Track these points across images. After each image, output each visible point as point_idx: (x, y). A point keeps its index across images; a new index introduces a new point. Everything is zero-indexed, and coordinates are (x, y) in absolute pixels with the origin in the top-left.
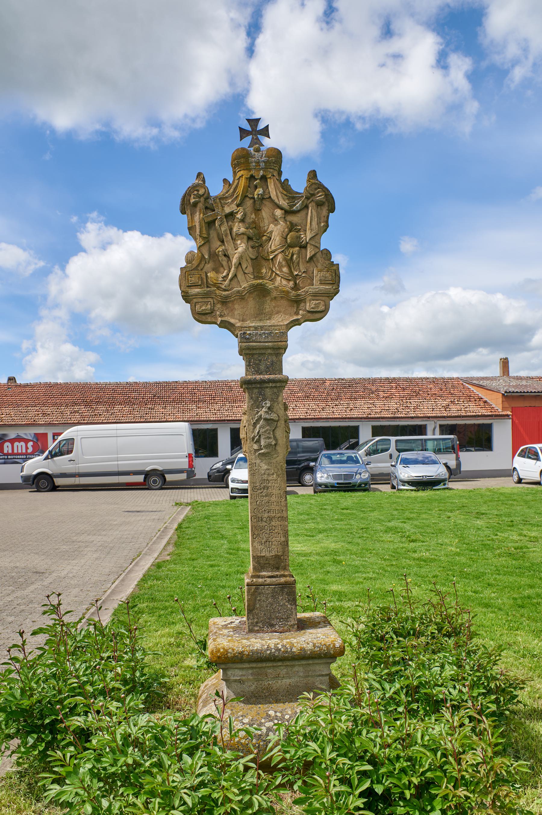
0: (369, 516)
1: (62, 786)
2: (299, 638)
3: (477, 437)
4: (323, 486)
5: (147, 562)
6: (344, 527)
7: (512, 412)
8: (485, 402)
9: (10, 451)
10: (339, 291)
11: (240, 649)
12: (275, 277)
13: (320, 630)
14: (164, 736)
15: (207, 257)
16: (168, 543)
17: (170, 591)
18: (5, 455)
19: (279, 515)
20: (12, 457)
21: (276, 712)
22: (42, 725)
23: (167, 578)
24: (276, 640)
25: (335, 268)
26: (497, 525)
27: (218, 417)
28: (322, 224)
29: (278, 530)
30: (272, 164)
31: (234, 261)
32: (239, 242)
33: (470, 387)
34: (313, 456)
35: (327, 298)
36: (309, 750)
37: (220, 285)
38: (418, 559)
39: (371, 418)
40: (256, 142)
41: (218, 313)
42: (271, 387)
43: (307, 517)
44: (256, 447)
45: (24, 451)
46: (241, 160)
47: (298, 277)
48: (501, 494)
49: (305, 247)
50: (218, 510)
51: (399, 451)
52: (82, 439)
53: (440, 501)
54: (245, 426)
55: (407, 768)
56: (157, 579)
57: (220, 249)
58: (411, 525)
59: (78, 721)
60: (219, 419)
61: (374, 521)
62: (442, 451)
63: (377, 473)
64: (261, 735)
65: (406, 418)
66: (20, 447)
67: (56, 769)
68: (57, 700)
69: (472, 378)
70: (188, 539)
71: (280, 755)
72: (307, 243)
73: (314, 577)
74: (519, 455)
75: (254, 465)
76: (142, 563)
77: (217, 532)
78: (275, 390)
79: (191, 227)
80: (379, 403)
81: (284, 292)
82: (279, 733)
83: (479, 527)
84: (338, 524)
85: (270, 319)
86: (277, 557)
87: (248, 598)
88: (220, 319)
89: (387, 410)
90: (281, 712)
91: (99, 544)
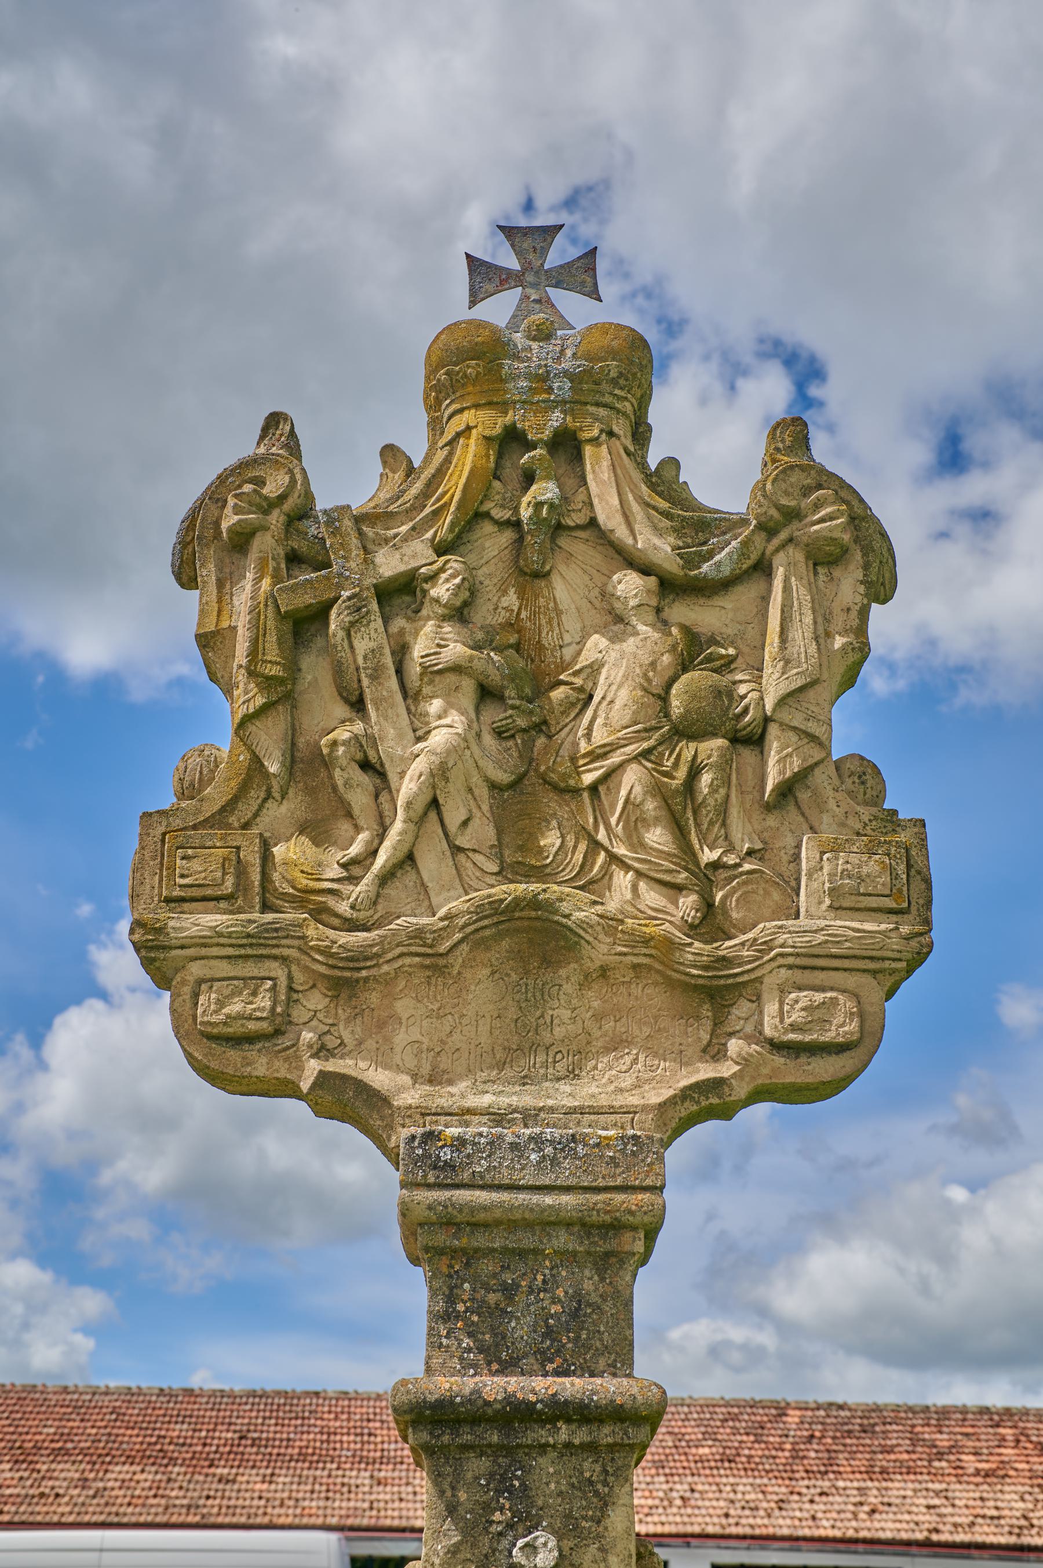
42: (568, 1445)
78: (590, 1468)
80: (964, 1494)
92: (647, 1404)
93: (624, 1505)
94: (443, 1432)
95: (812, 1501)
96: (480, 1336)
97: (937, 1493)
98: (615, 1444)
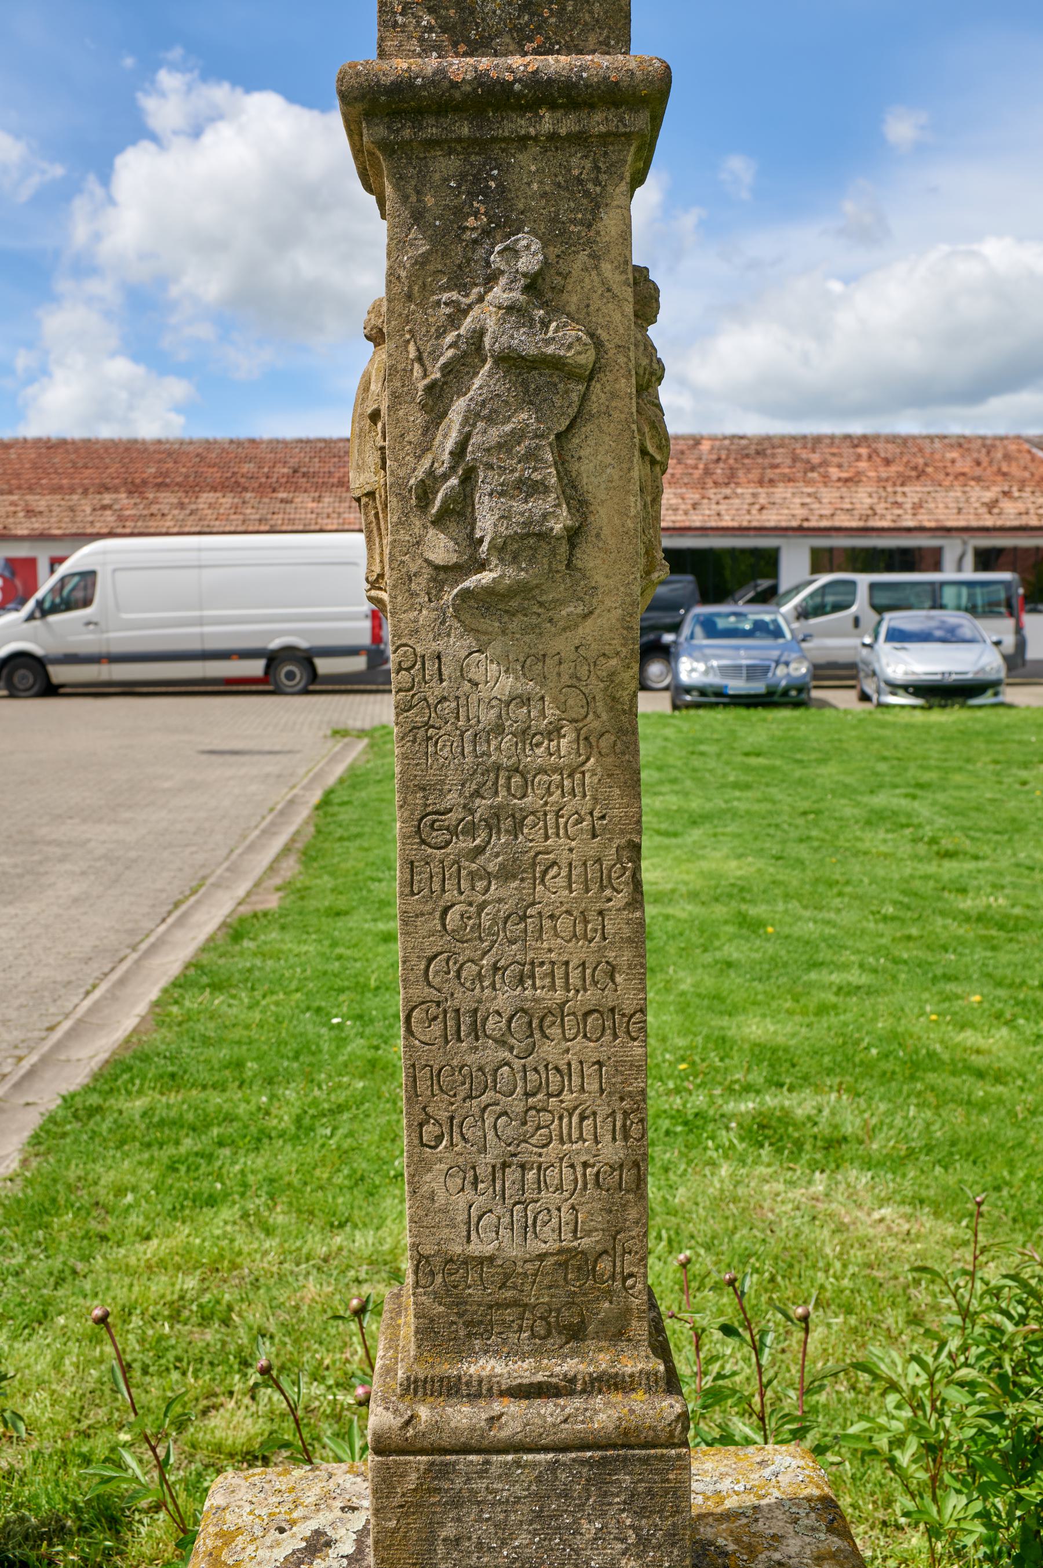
0: (818, 775)
6: (756, 807)
16: (286, 850)
19: (590, 997)
34: (668, 619)
42: (553, 137)
44: (441, 548)
51: (880, 609)
52: (118, 574)
53: (990, 735)
62: (980, 609)
70: (341, 839)
75: (431, 668)
76: (198, 917)
78: (579, 164)
80: (828, 495)
84: (739, 799)
86: (572, 1262)
92: (648, 81)
93: (619, 207)
94: (403, 126)
95: (718, 503)
96: (443, 12)
97: (809, 495)
98: (608, 134)
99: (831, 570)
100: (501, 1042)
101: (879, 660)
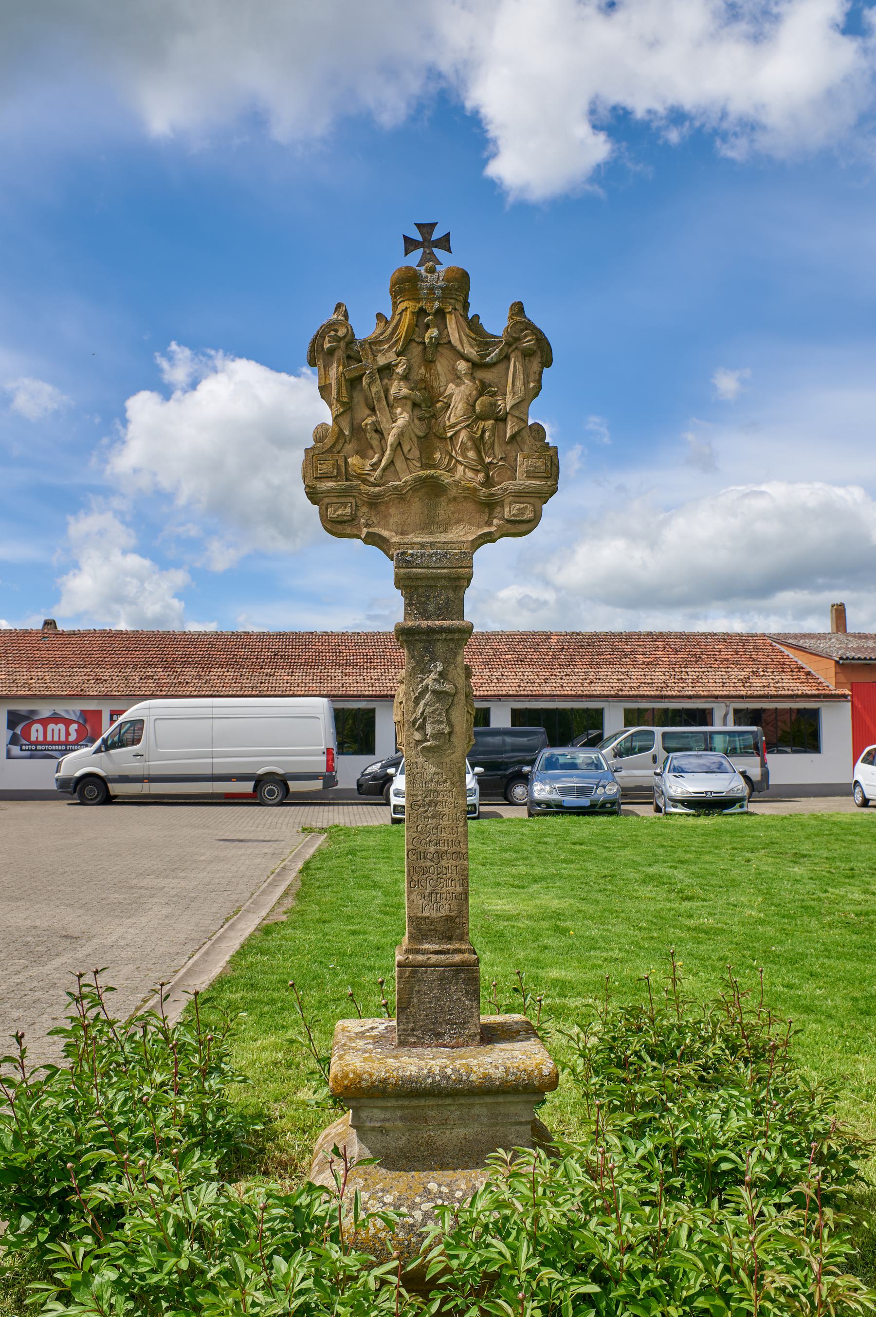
0: (617, 856)
1: (67, 1305)
2: (481, 1058)
3: (799, 731)
4: (542, 806)
5: (249, 924)
7: (851, 690)
8: (808, 674)
9: (41, 739)
10: (557, 489)
11: (383, 1075)
12: (455, 465)
13: (518, 1045)
14: (245, 1223)
15: (347, 433)
16: (286, 894)
17: (282, 973)
18: (32, 743)
19: (454, 849)
20: (43, 747)
21: (440, 1185)
22: (46, 1196)
23: (279, 951)
24: (444, 1060)
25: (551, 453)
26: (827, 875)
27: (376, 690)
28: (532, 385)
29: (453, 873)
30: (453, 292)
31: (391, 439)
32: (399, 410)
33: (782, 648)
35: (537, 500)
36: (492, 1254)
37: (368, 478)
38: (694, 929)
39: (622, 696)
40: (429, 257)
41: (362, 521)
42: (445, 639)
43: (515, 855)
44: (418, 736)
45: (63, 739)
46: (406, 285)
47: (493, 466)
48: (834, 823)
49: (504, 420)
50: (371, 842)
51: (668, 750)
52: (157, 722)
53: (734, 833)
54: (401, 703)
55: (661, 1291)
56: (263, 953)
57: (369, 421)
58: (686, 872)
59: (100, 1192)
60: (378, 693)
61: (625, 865)
62: (739, 751)
63: (632, 785)
64: (413, 1225)
65: (679, 697)
66: (56, 731)
67: (58, 1275)
68: (73, 1153)
69: (787, 636)
71: (440, 1262)
72: (507, 413)
73: (521, 955)
74: (864, 761)
75: (415, 765)
76: (240, 926)
77: (367, 877)
78: (452, 645)
79: (325, 386)
80: (635, 673)
81: (468, 489)
82: (443, 1222)
83: (798, 878)
84: (565, 869)
85: (445, 531)
86: (448, 918)
87: (399, 988)
88: (365, 530)
89: (649, 684)
90: (448, 1185)
91: (173, 892)
92: (468, 628)
97: (623, 673)
99: (639, 725)
100: (431, 860)
101: (665, 785)
